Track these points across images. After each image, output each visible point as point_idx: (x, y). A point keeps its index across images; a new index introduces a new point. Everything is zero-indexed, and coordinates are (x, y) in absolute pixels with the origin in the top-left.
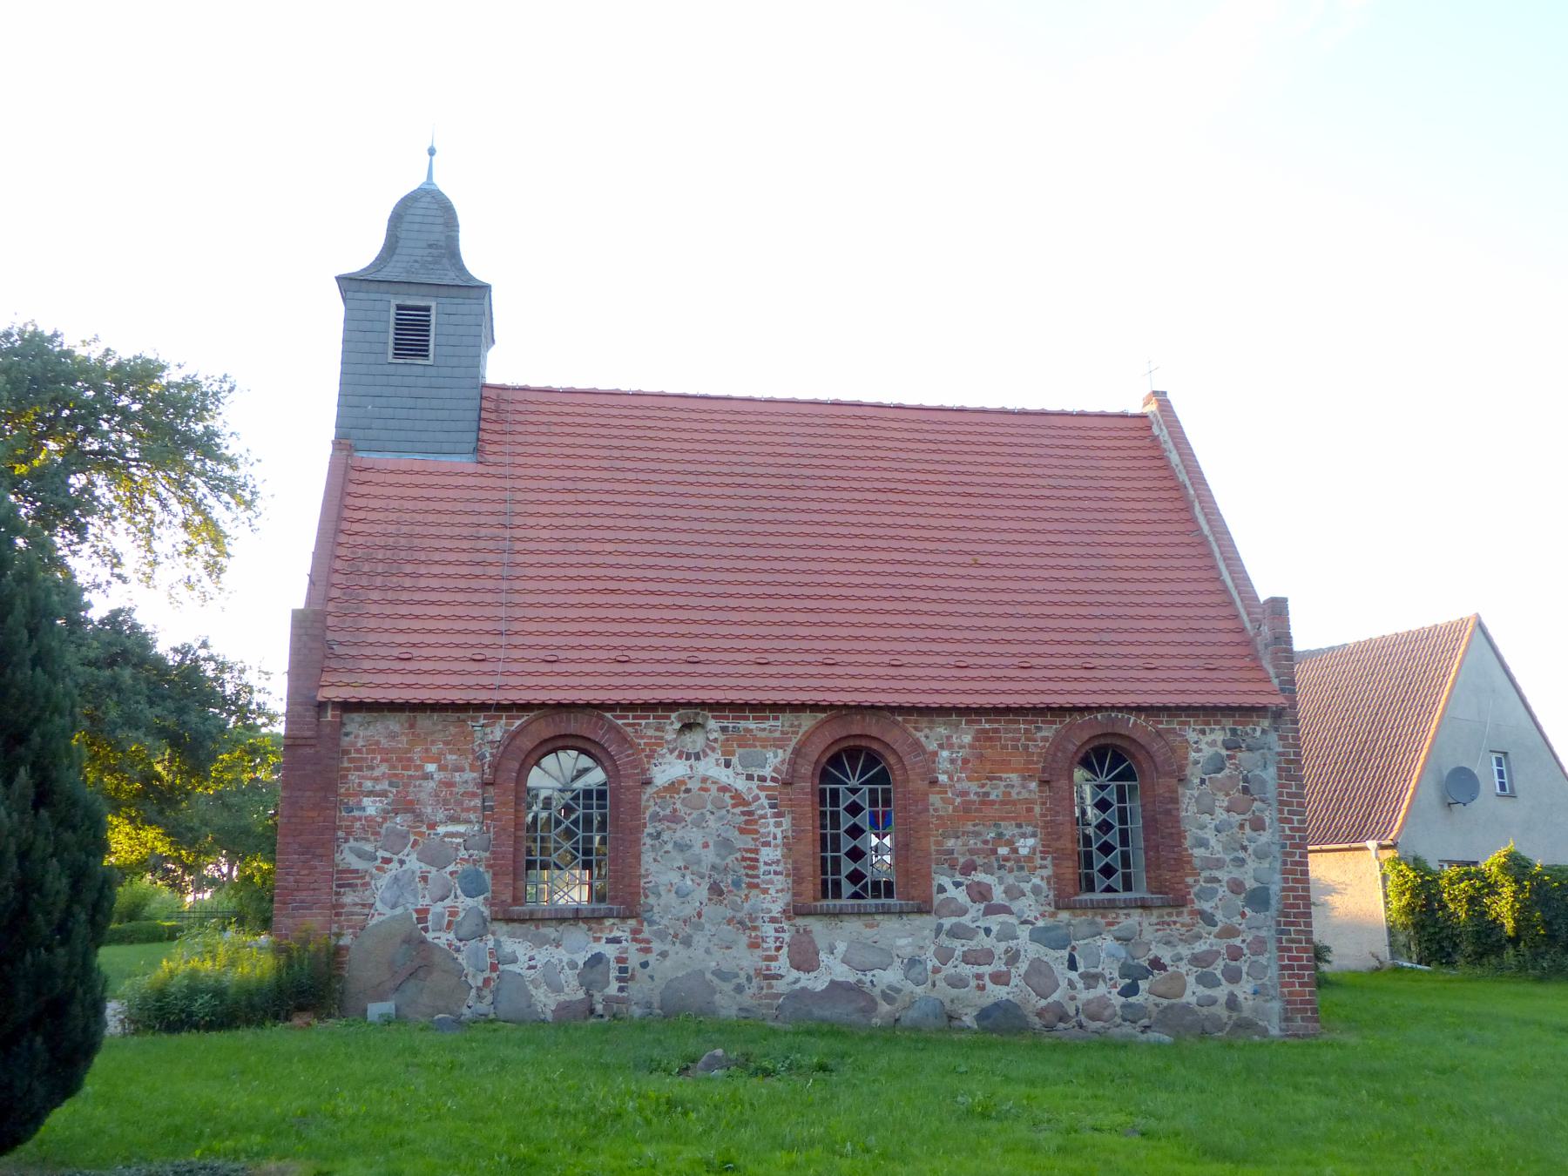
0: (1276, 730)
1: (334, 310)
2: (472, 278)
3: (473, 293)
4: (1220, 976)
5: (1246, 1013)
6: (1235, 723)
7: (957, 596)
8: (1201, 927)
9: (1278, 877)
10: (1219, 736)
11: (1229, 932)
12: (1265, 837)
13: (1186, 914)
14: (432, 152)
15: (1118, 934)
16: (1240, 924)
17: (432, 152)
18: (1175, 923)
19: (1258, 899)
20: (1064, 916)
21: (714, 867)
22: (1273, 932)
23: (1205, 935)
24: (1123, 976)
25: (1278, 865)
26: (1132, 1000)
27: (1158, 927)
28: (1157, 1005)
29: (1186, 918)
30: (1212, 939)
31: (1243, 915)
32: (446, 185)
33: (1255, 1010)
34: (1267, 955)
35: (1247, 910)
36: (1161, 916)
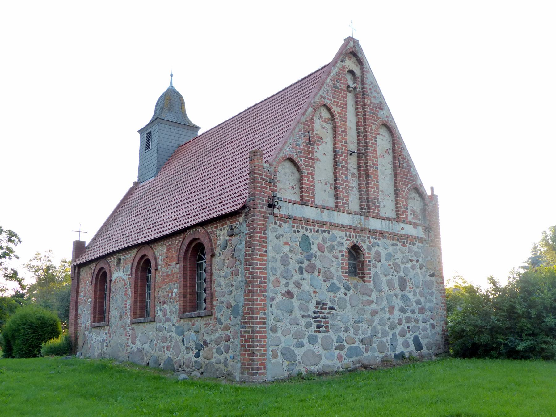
0: (246, 222)
1: (138, 135)
2: (191, 123)
3: (195, 129)
4: (223, 350)
5: (230, 368)
6: (232, 222)
7: (184, 180)
8: (218, 326)
9: (242, 298)
10: (226, 230)
11: (226, 328)
12: (239, 279)
13: (213, 319)
14: (172, 75)
15: (195, 329)
16: (229, 324)
17: (172, 75)
18: (210, 323)
19: (234, 310)
20: (182, 321)
21: (314, 313)
22: (239, 328)
23: (219, 329)
24: (196, 348)
25: (243, 292)
26: (197, 359)
27: (206, 326)
28: (205, 362)
29: (213, 322)
30: (221, 332)
31: (230, 319)
32: (178, 88)
33: (232, 367)
34: (237, 340)
35: (232, 317)
36: (206, 321)
